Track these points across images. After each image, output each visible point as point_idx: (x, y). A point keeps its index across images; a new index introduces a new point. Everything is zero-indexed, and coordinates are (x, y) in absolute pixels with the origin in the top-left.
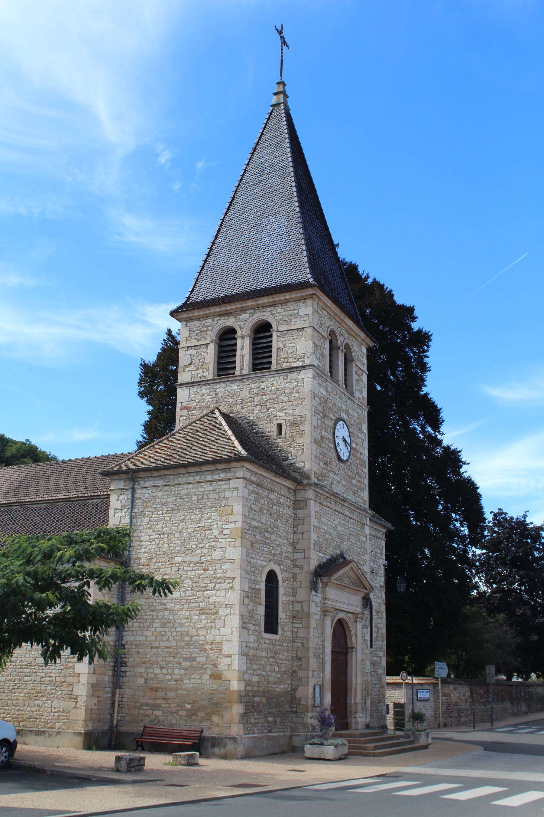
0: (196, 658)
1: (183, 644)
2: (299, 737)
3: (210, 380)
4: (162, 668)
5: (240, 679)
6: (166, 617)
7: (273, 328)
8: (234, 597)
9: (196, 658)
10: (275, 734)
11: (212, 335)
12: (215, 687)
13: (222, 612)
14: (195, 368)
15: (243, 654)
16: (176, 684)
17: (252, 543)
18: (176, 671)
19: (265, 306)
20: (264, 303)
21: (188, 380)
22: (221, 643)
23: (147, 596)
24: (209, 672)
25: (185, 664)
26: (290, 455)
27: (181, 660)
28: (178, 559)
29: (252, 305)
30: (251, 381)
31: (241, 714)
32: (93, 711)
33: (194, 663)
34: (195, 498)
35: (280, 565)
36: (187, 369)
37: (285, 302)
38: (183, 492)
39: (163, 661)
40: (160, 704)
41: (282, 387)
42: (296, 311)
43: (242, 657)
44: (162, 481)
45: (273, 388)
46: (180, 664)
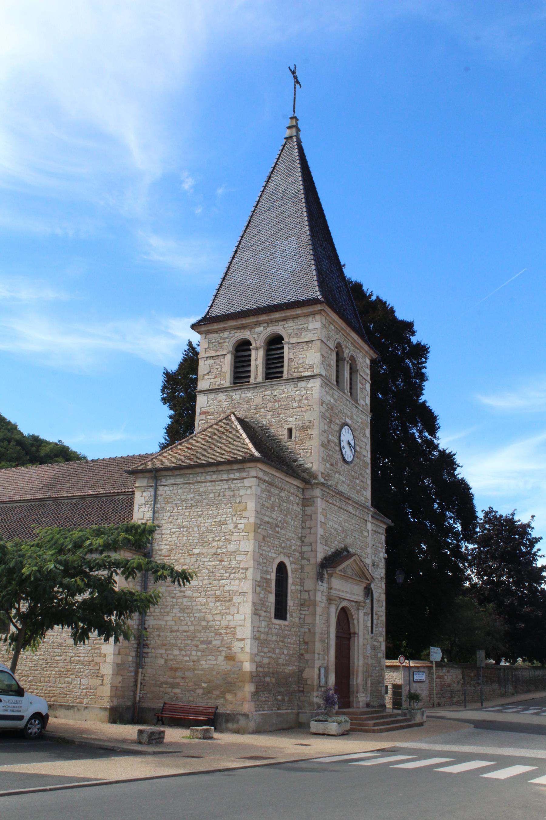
0: (211, 641)
1: (200, 628)
8: (247, 586)
9: (211, 641)
11: (229, 346)
13: (237, 599)
14: (213, 377)
15: (255, 638)
16: (194, 665)
17: (264, 537)
18: (194, 653)
19: (278, 321)
20: (278, 318)
22: (235, 628)
24: (224, 654)
28: (196, 551)
30: (264, 389)
31: (252, 693)
34: (212, 495)
35: (289, 557)
37: (297, 317)
38: (201, 490)
42: (306, 325)
45: (285, 395)
46: (197, 646)
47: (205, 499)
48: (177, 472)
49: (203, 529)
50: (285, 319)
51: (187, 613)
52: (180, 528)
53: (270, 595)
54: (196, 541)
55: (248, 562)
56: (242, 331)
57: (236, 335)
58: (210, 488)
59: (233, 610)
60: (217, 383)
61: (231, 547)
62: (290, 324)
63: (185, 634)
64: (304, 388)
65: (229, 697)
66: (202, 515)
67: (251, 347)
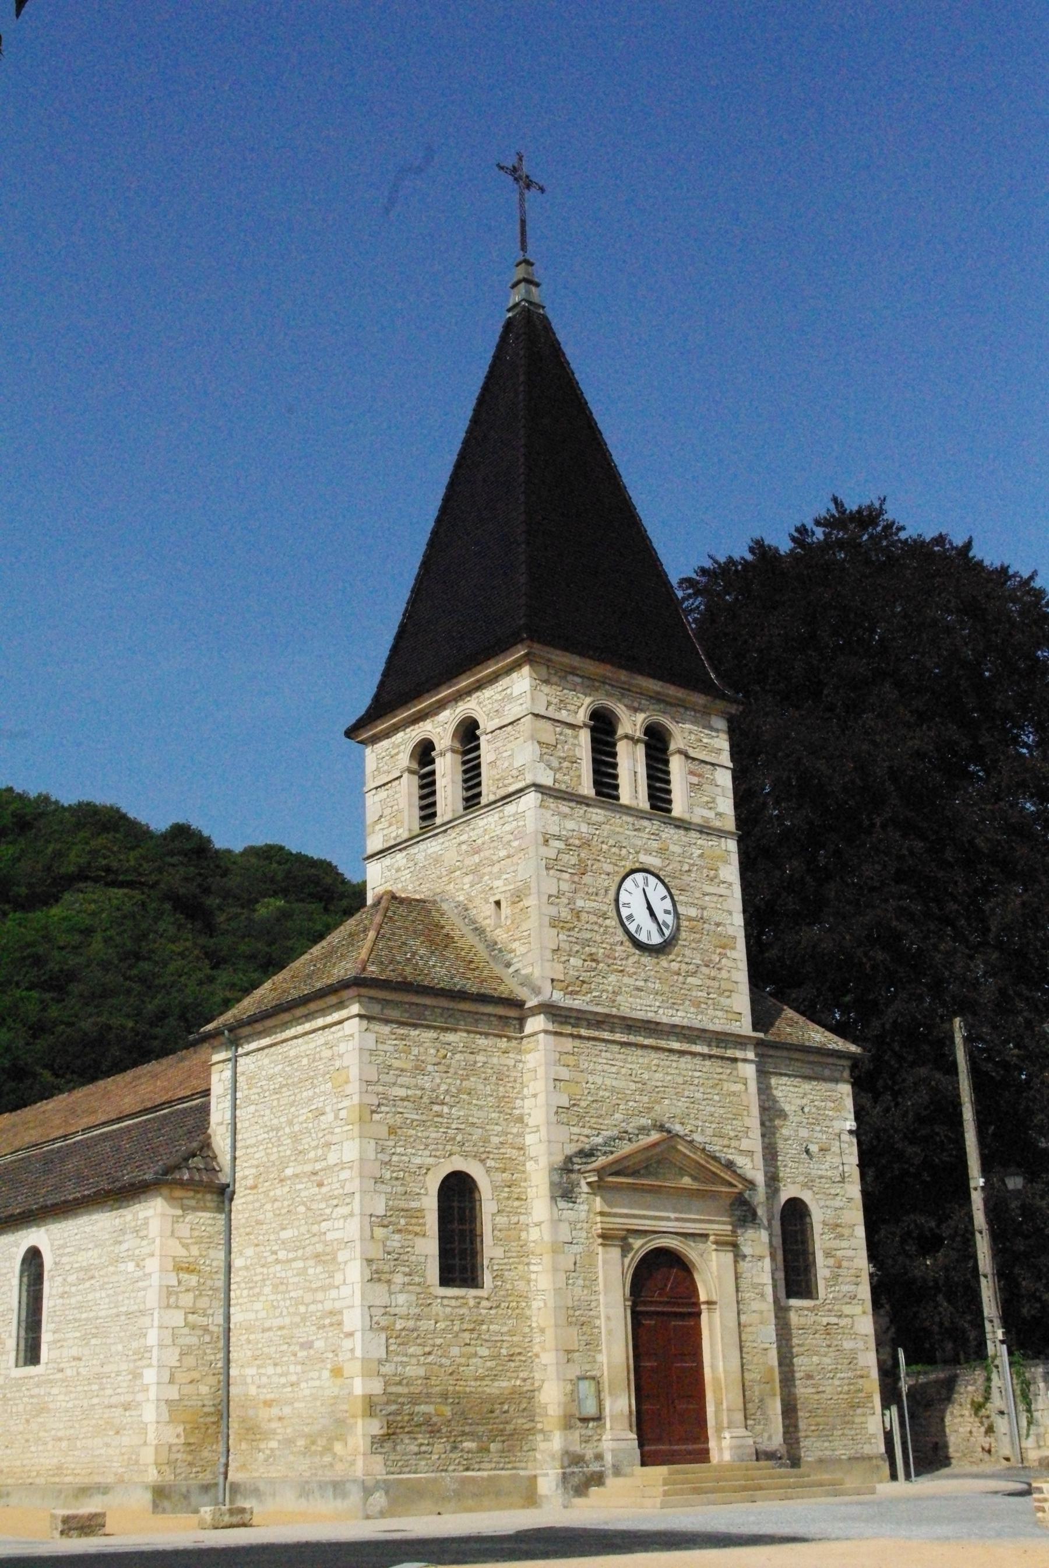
0: (312, 1342)
1: (297, 1319)
2: (547, 1479)
3: (406, 841)
4: (276, 1365)
5: (366, 1374)
6: (278, 1275)
7: (482, 726)
8: (353, 1229)
9: (312, 1342)
10: (485, 1474)
12: (336, 1391)
13: (342, 1256)
14: (386, 824)
15: (374, 1327)
16: (292, 1392)
17: (392, 1130)
18: (292, 1368)
19: (469, 692)
20: (466, 687)
21: (380, 847)
22: (341, 1312)
23: (256, 1241)
24: (329, 1366)
25: (302, 1354)
26: (512, 955)
27: (297, 1348)
28: (289, 1172)
29: (449, 695)
30: (457, 830)
31: (374, 1437)
32: (174, 1449)
33: (312, 1352)
34: (305, 1061)
35: (482, 1161)
36: (378, 827)
38: (292, 1053)
39: (276, 1352)
40: (275, 1430)
41: (498, 833)
42: (509, 691)
43: (370, 1335)
44: (268, 1039)
45: (487, 837)
46: (295, 1355)
47: (297, 1070)
48: (259, 1027)
49: (297, 1128)
50: (479, 686)
51: (282, 1293)
52: (268, 1132)
53: (419, 1242)
54: (288, 1152)
55: (350, 1180)
56: (421, 724)
57: (414, 733)
58: (303, 1048)
59: (338, 1278)
60: (394, 835)
61: (332, 1158)
62: (487, 693)
63: (279, 1333)
64: (514, 815)
65: (338, 1447)
66: (294, 1101)
67: (433, 754)
